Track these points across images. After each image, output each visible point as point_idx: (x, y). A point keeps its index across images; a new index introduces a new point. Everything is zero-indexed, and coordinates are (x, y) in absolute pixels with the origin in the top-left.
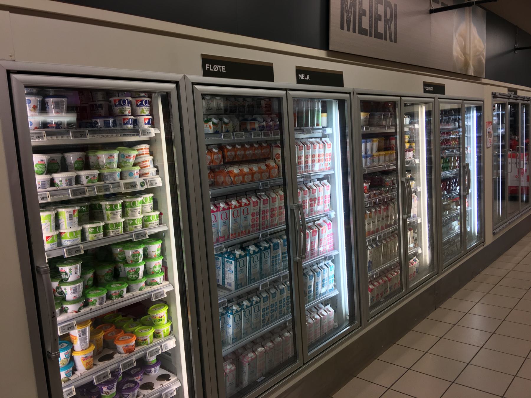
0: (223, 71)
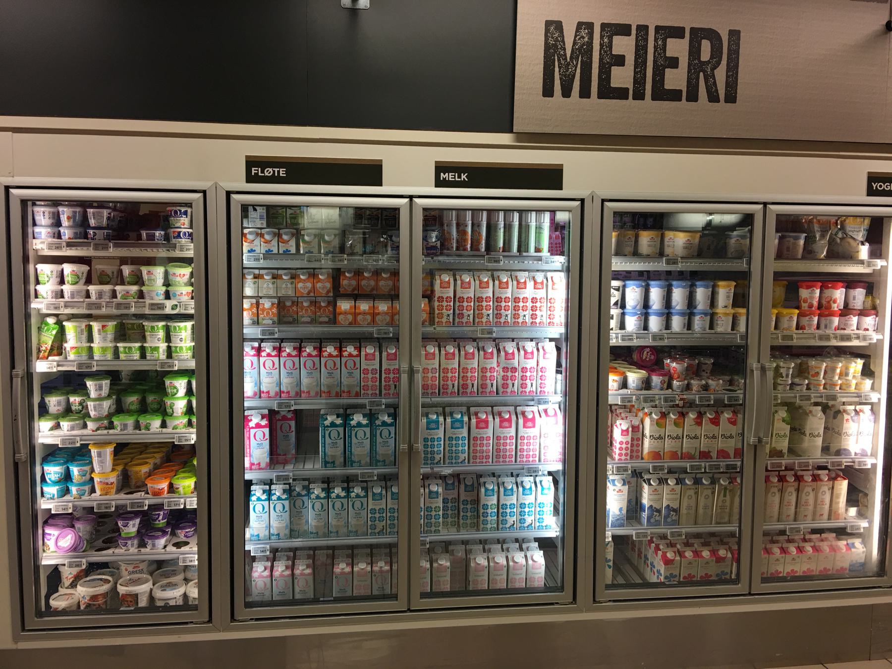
0: (281, 175)
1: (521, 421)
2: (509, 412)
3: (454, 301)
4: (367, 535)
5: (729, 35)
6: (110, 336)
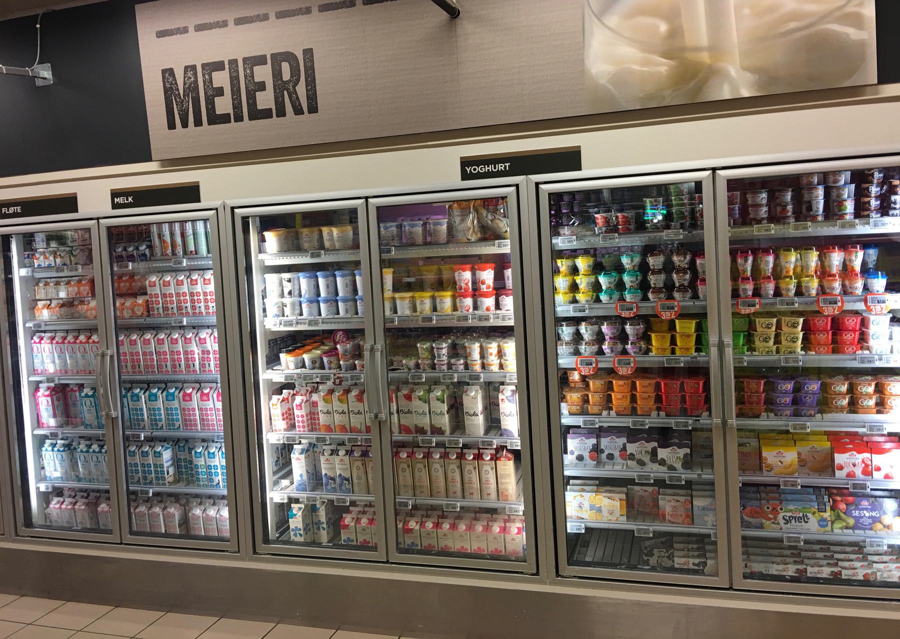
5: (303, 54)
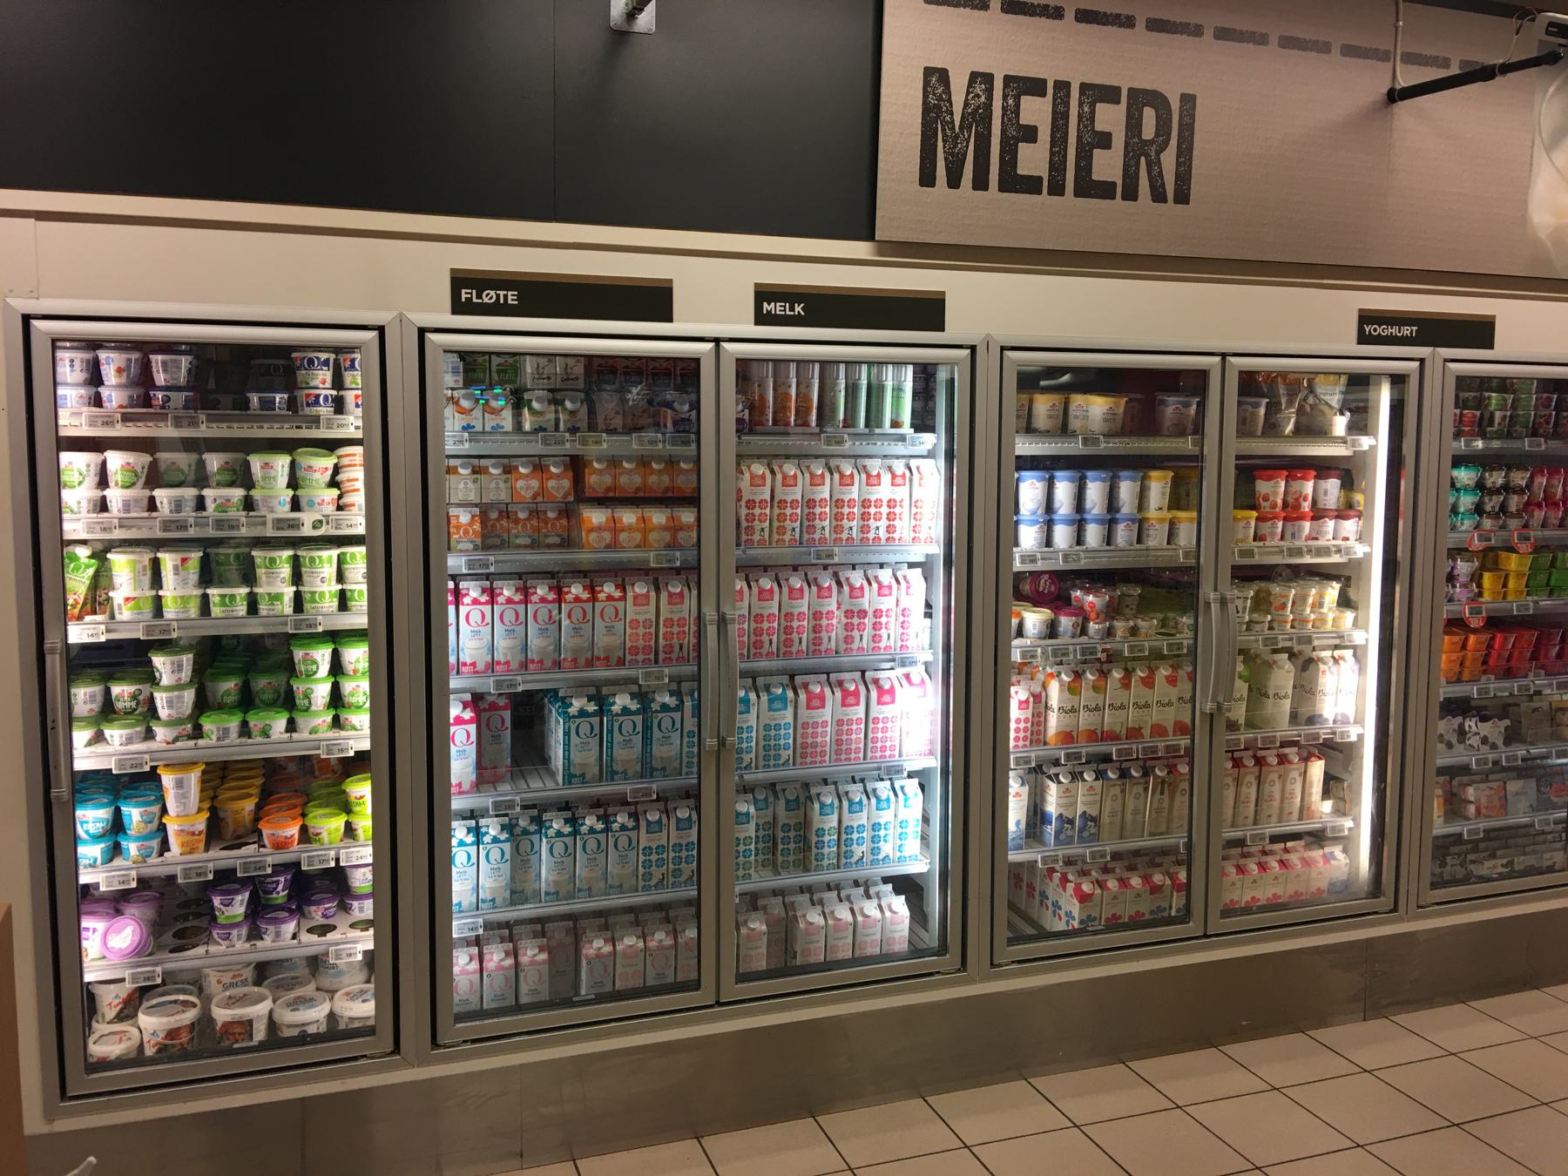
0: (510, 302)
1: (874, 694)
2: (854, 680)
3: (772, 507)
4: (637, 891)
5: (1181, 102)
6: (193, 576)
